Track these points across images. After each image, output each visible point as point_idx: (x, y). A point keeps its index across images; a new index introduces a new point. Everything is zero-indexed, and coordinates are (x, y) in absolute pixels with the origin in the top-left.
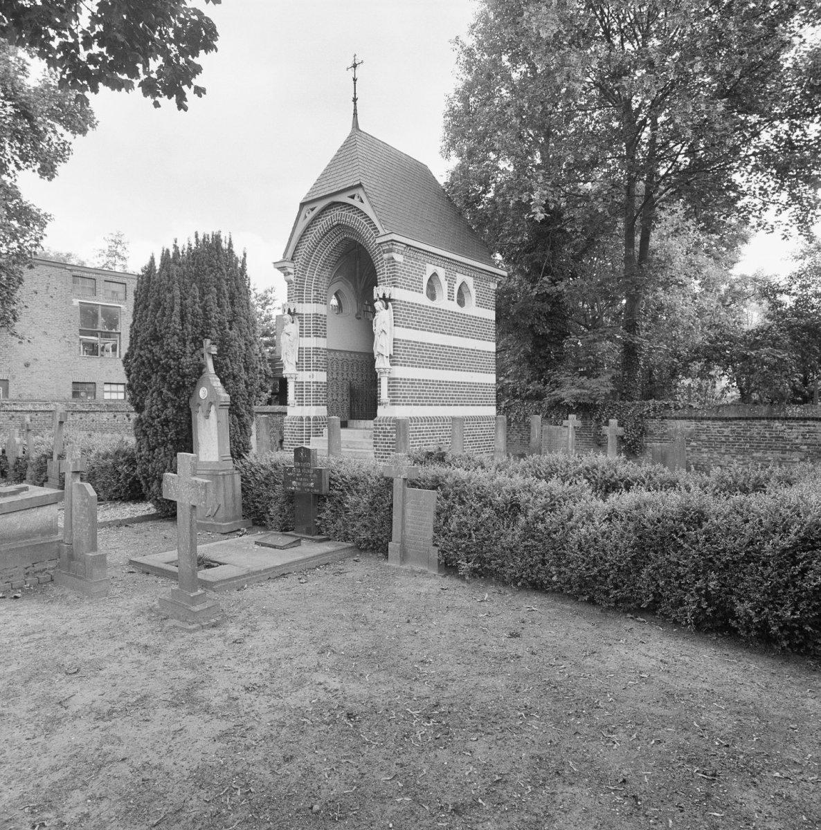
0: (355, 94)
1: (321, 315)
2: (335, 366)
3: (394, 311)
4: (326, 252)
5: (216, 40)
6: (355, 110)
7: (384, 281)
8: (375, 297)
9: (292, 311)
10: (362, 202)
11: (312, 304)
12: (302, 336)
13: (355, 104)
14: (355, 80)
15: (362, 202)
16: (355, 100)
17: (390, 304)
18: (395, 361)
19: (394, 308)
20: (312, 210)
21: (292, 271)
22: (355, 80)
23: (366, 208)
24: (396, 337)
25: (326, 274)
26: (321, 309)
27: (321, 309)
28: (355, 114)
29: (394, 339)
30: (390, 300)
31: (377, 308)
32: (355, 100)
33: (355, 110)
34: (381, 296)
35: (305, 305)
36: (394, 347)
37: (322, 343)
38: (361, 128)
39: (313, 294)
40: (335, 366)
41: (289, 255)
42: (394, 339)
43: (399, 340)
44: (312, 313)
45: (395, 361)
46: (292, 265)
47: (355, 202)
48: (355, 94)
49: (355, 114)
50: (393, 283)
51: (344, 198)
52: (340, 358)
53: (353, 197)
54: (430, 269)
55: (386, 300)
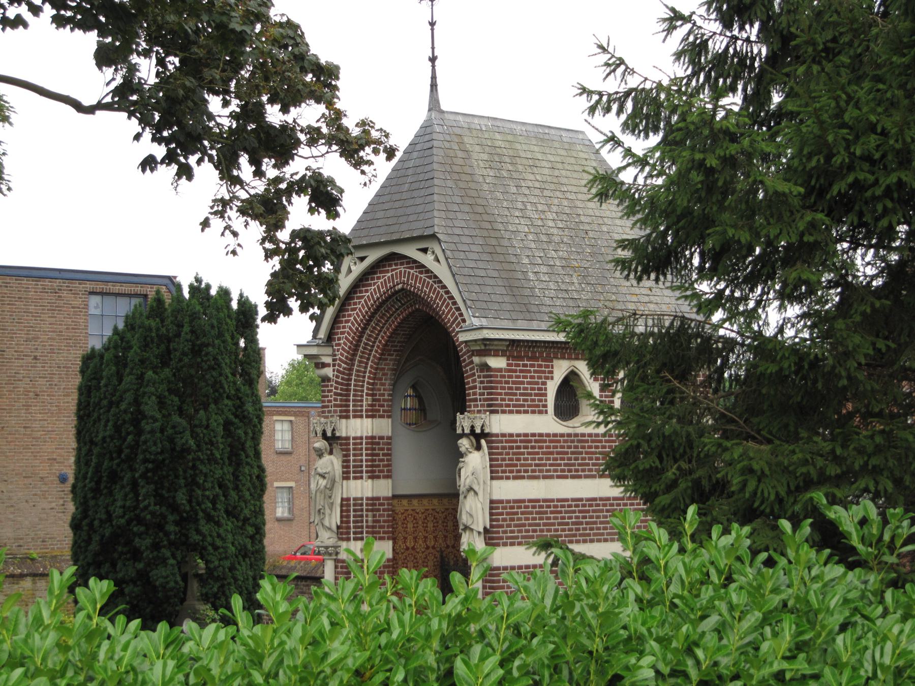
0: (433, 48)
1: (381, 438)
2: (410, 526)
3: (490, 454)
4: (382, 339)
5: (284, 315)
6: (434, 77)
7: (476, 400)
8: (459, 431)
9: (329, 434)
10: (438, 261)
11: (365, 420)
12: (348, 478)
13: (433, 67)
14: (432, 24)
15: (438, 261)
16: (433, 59)
17: (483, 442)
18: (493, 538)
19: (490, 448)
20: (362, 259)
21: (328, 360)
22: (432, 24)
23: (441, 271)
24: (495, 497)
25: (389, 365)
26: (382, 427)
27: (382, 427)
28: (434, 86)
29: (492, 502)
30: (484, 435)
31: (463, 449)
32: (433, 59)
33: (434, 77)
34: (467, 431)
35: (352, 421)
36: (491, 514)
37: (383, 488)
38: (444, 107)
39: (366, 402)
40: (410, 526)
41: (322, 335)
42: (492, 502)
43: (501, 502)
44: (365, 435)
45: (493, 538)
46: (329, 351)
47: (427, 260)
48: (433, 48)
49: (434, 86)
50: (489, 405)
51: (410, 251)
52: (422, 509)
53: (425, 251)
54: (561, 369)
55: (478, 437)
